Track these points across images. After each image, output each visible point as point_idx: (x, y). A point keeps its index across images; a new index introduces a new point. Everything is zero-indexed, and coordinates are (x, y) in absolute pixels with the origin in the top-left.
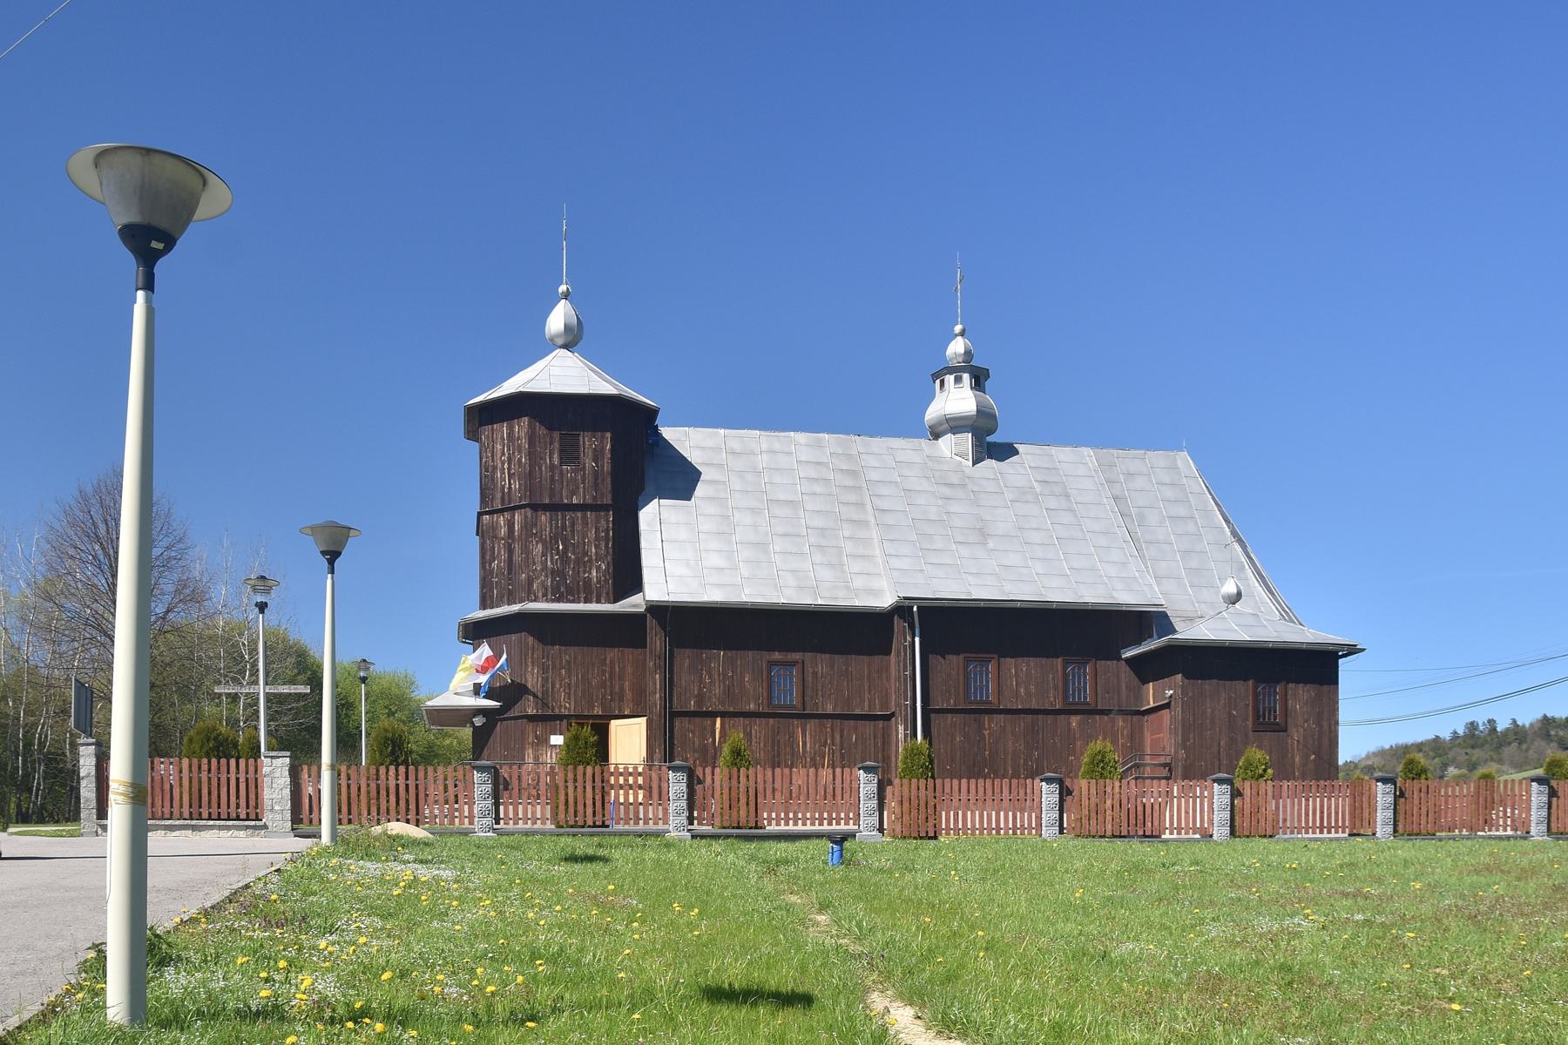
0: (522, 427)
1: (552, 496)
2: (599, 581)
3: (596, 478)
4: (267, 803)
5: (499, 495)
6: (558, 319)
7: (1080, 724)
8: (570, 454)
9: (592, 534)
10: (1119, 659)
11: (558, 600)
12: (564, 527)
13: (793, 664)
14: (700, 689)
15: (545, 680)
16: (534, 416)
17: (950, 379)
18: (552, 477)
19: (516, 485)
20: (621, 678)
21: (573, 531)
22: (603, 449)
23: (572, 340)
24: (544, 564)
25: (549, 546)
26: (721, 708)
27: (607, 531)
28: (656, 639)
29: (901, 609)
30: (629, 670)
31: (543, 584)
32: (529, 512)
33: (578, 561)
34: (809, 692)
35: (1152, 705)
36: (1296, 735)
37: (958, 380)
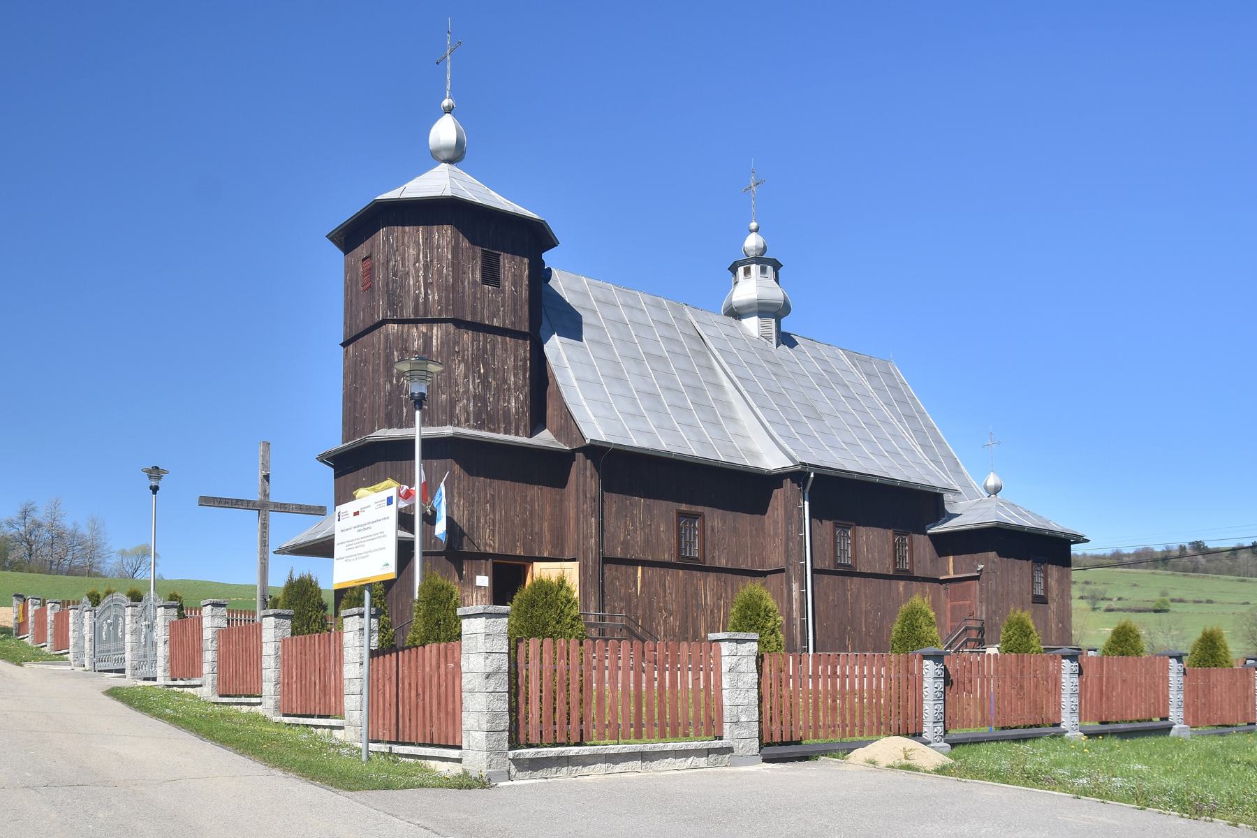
0: (444, 236)
1: (474, 314)
2: (517, 413)
3: (515, 304)
4: (346, 659)
5: (411, 304)
6: (444, 132)
7: (905, 586)
8: (491, 275)
9: (511, 362)
10: (925, 534)
11: (480, 428)
12: (485, 351)
13: (696, 516)
14: (625, 536)
15: (471, 514)
16: (461, 227)
17: (755, 268)
18: (475, 293)
19: (434, 296)
20: (541, 518)
21: (493, 355)
22: (521, 276)
23: (456, 156)
24: (466, 386)
25: (471, 367)
26: (641, 557)
27: (525, 360)
28: (583, 476)
29: (798, 475)
30: (548, 509)
31: (466, 409)
32: (451, 327)
33: (498, 388)
34: (708, 545)
35: (952, 576)
36: (1053, 606)
37: (763, 270)
